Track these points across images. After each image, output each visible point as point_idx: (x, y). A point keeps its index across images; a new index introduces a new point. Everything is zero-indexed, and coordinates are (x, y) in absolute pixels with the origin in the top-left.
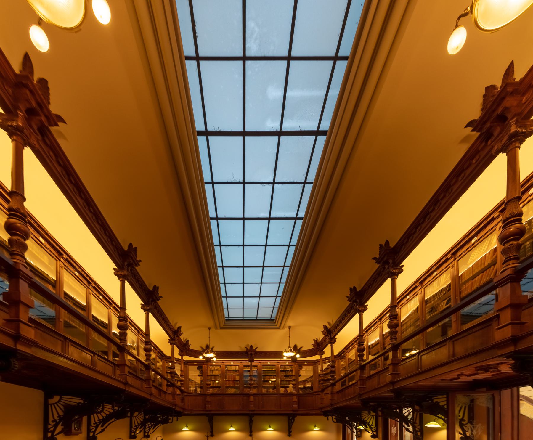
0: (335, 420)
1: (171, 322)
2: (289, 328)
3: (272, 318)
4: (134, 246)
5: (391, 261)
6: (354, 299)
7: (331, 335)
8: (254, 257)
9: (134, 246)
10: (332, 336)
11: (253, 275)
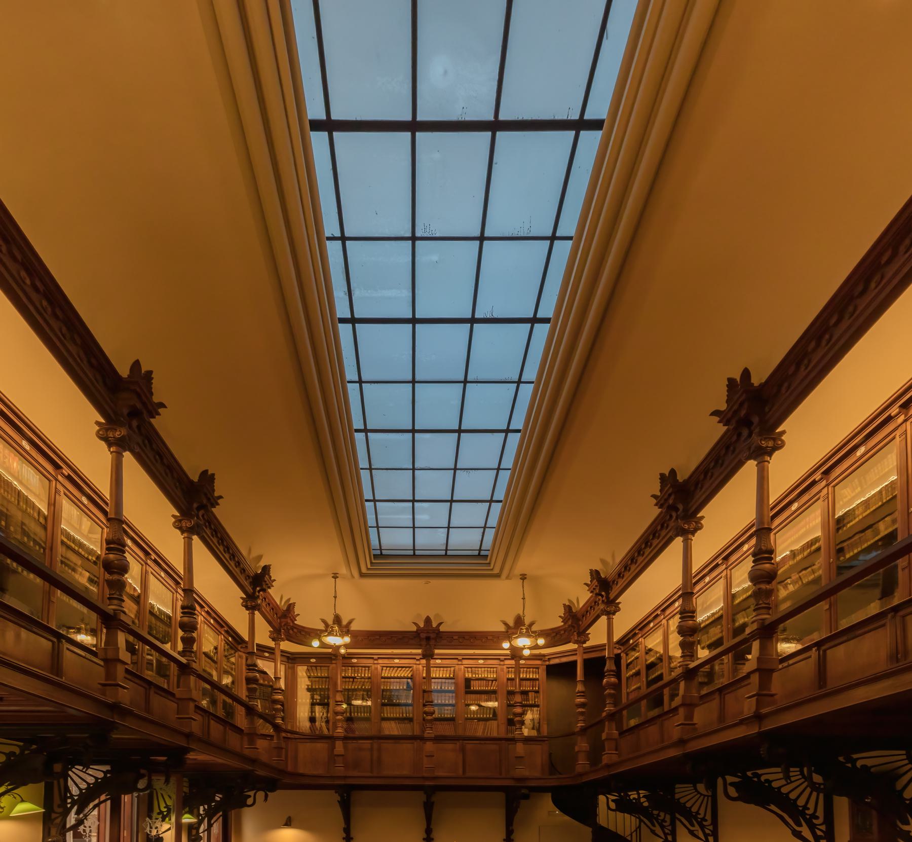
0: (613, 805)
1: (244, 552)
2: (523, 577)
3: (483, 553)
4: (144, 369)
5: (756, 420)
6: (671, 502)
7: (608, 594)
8: (438, 405)
9: (144, 369)
10: (612, 596)
11: (435, 450)
